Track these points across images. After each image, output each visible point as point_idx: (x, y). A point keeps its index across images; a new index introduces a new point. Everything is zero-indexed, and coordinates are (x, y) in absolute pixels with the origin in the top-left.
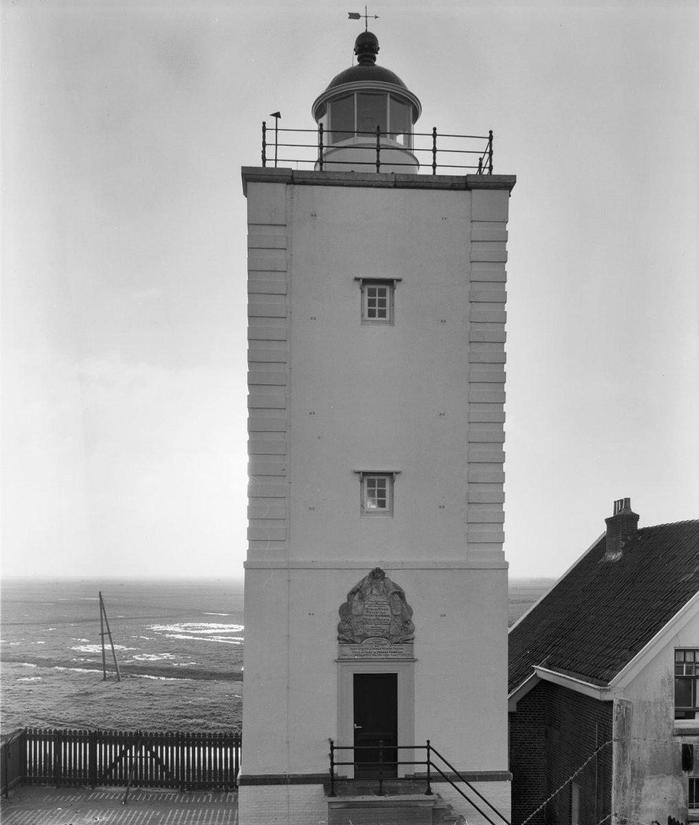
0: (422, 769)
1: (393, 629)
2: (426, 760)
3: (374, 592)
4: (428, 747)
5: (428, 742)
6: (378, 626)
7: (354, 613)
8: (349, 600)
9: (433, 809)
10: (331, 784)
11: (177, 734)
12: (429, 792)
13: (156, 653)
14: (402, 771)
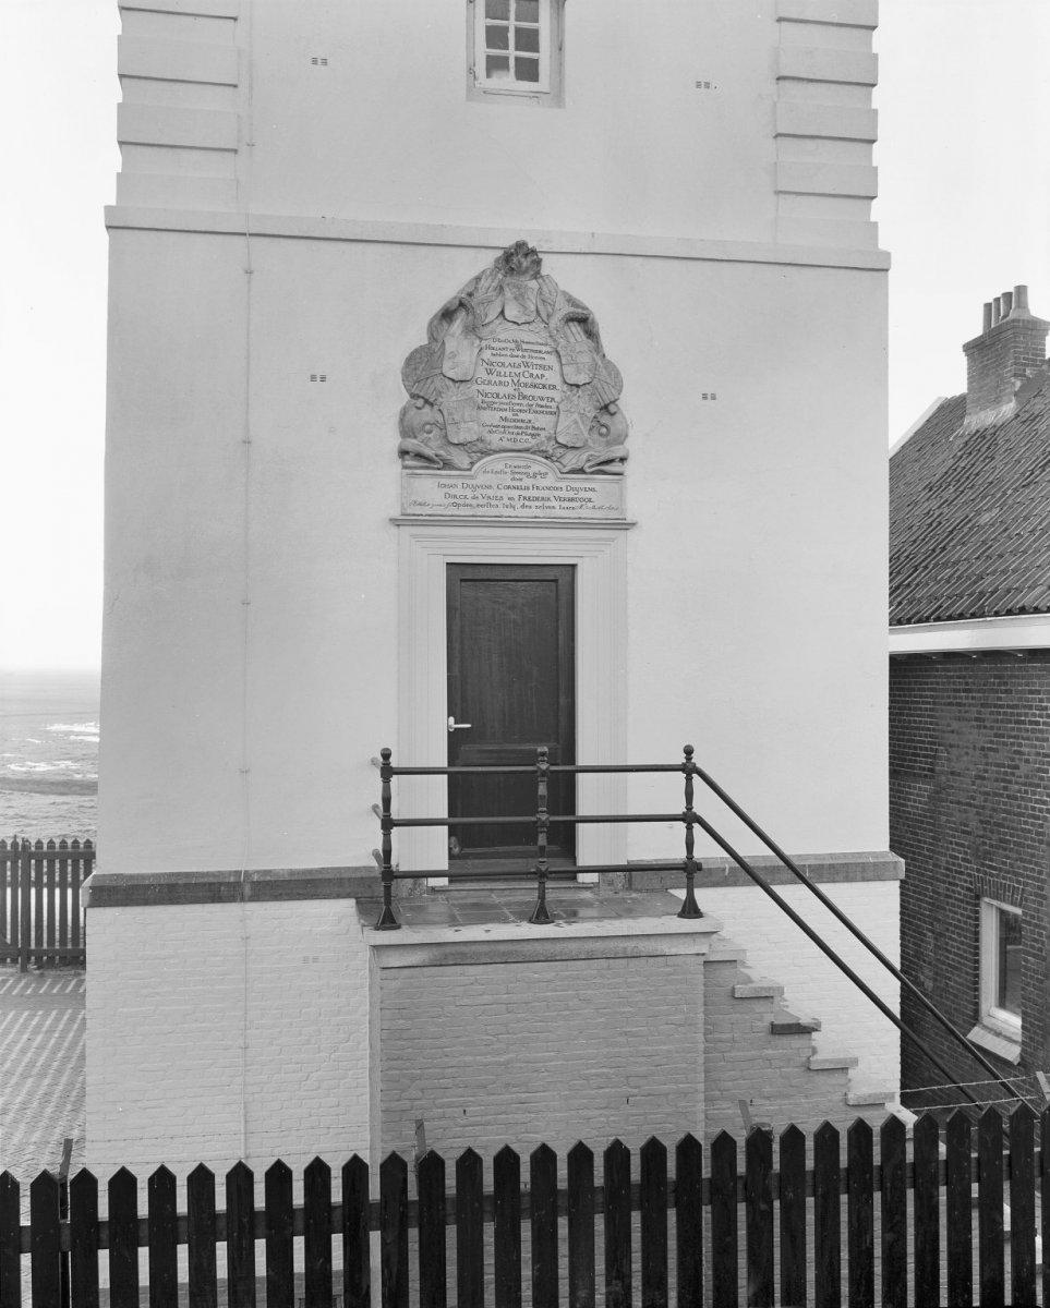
0: (665, 844)
1: (570, 427)
2: (681, 809)
3: (511, 313)
4: (689, 769)
5: (689, 751)
6: (522, 416)
7: (450, 374)
8: (433, 338)
9: (706, 963)
10: (382, 895)
11: (15, 844)
12: (691, 910)
13: (49, 761)
14: (592, 846)
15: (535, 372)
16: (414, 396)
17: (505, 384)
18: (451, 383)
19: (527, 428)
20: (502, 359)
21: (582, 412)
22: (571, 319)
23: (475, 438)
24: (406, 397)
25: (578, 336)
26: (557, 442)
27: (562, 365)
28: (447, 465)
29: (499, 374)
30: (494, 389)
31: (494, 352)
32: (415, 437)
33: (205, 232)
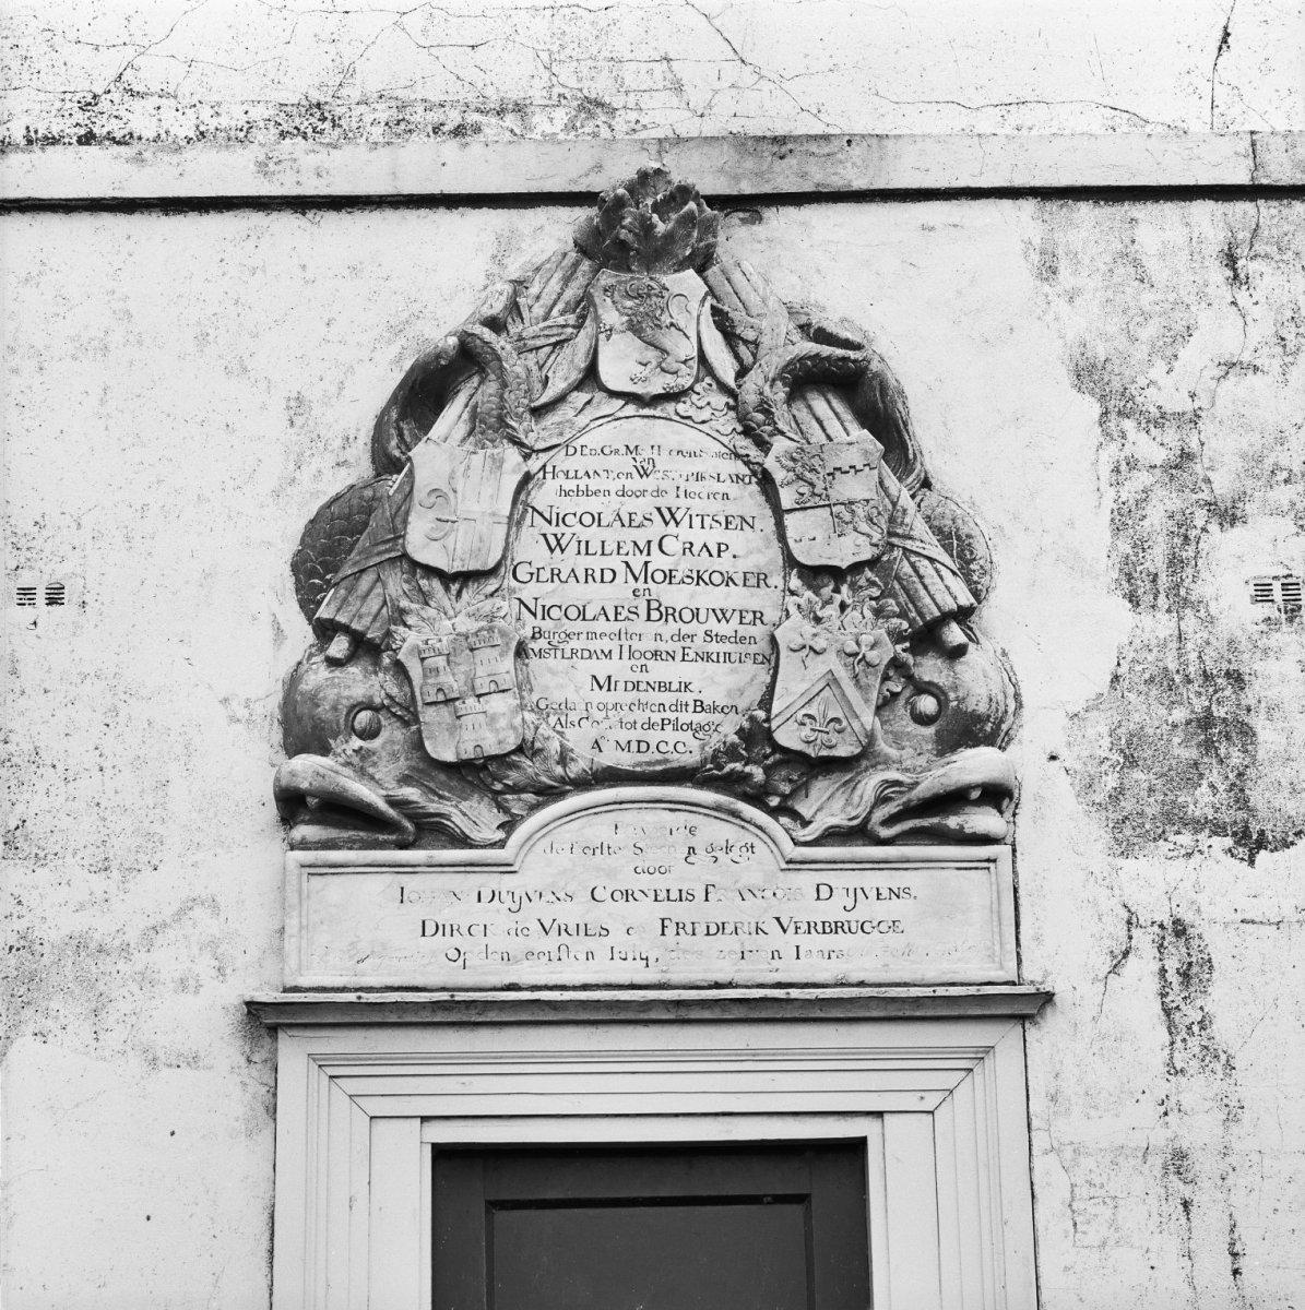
6: (659, 671)
8: (387, 463)
15: (698, 537)
16: (325, 631)
17: (606, 577)
18: (436, 584)
19: (680, 706)
20: (594, 504)
21: (851, 647)
22: (805, 379)
23: (511, 743)
24: (301, 633)
25: (834, 427)
26: (777, 748)
27: (779, 513)
28: (430, 830)
29: (585, 548)
30: (575, 593)
31: (570, 485)
32: (325, 751)
33: (677, 1115)
